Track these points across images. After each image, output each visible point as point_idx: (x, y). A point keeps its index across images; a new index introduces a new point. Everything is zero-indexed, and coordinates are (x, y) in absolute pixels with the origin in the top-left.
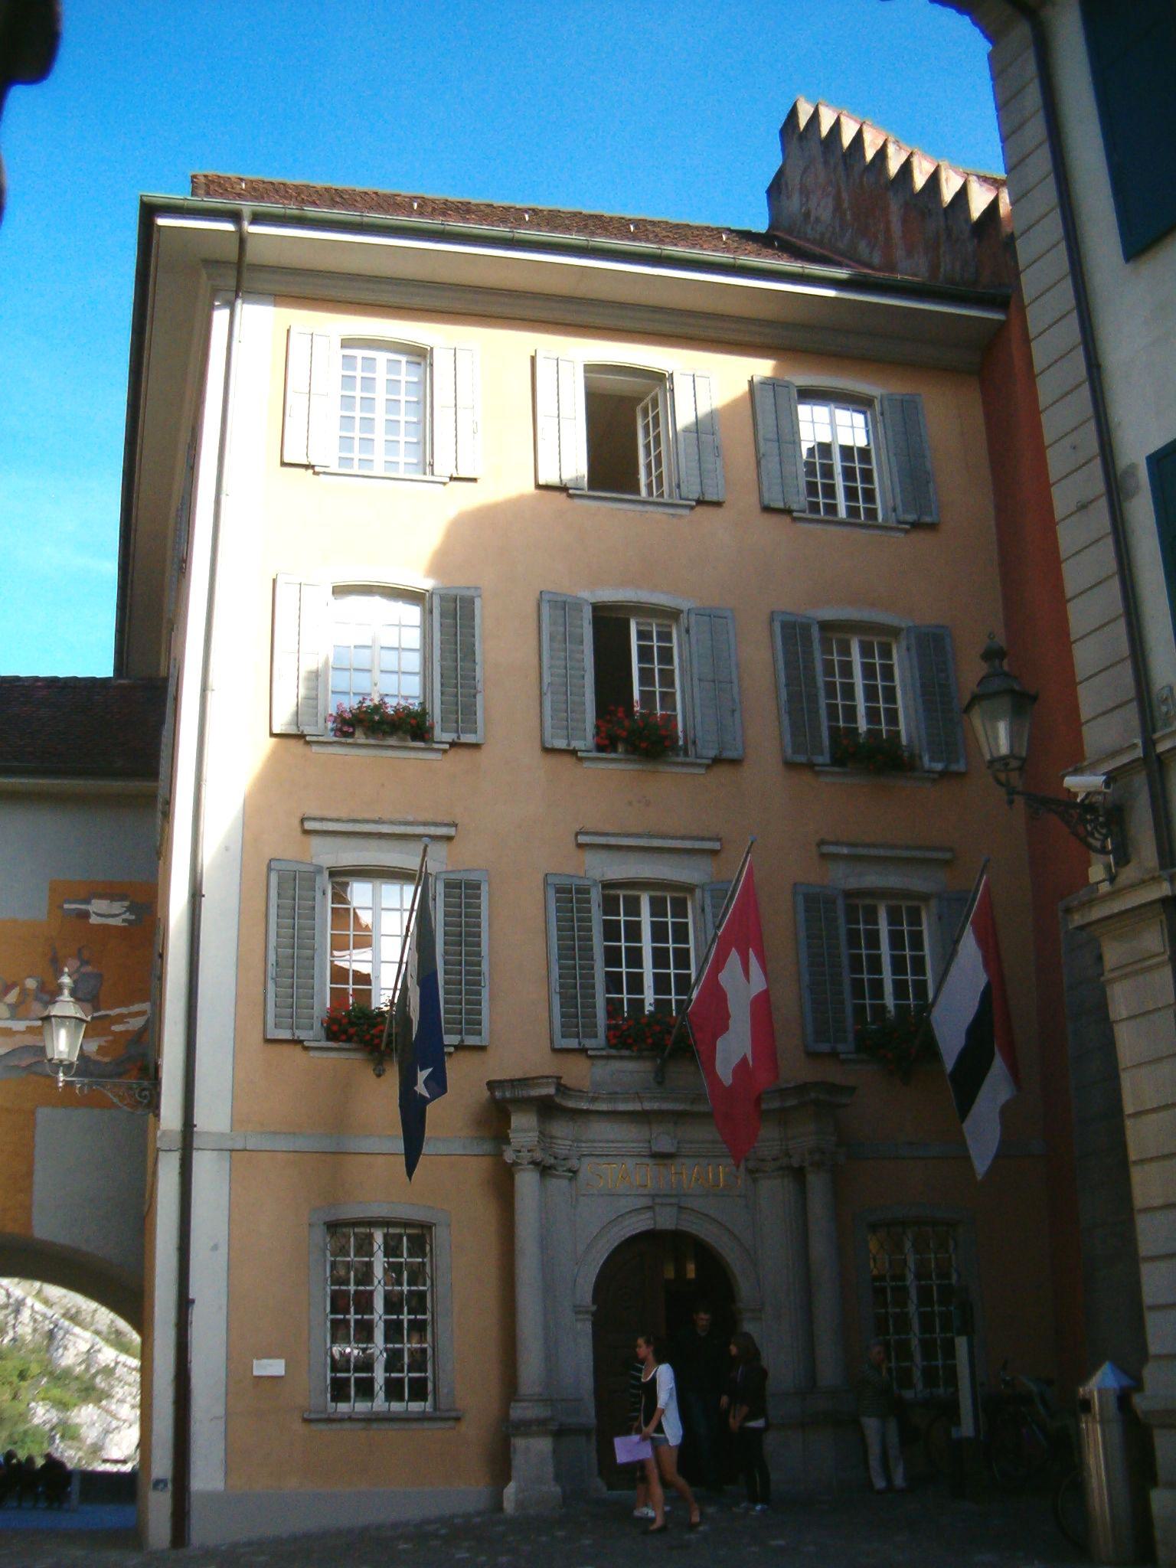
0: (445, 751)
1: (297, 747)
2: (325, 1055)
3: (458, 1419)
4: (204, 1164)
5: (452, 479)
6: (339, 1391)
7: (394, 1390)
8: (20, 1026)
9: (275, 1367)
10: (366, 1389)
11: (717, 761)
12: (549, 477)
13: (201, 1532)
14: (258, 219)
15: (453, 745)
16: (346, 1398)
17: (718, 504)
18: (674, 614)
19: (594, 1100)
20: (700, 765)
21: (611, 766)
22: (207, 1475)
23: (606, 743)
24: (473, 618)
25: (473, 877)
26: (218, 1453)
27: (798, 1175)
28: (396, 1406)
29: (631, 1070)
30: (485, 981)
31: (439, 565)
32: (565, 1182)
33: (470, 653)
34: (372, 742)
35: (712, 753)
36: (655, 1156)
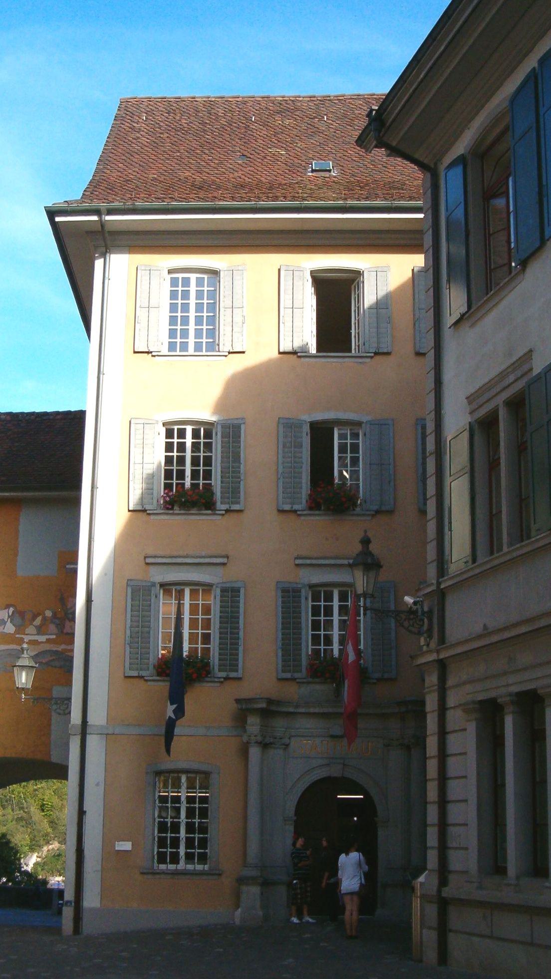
0: (223, 515)
1: (142, 516)
2: (156, 683)
3: (220, 875)
4: (93, 741)
5: (229, 353)
6: (162, 859)
7: (189, 857)
8: (42, 638)
9: (127, 846)
10: (175, 859)
11: (378, 512)
12: (286, 346)
13: (89, 926)
14: (110, 212)
15: (227, 511)
16: (165, 862)
17: (388, 354)
18: (359, 424)
19: (297, 707)
20: (368, 515)
21: (317, 518)
22: (91, 900)
23: (314, 505)
24: (240, 437)
25: (236, 585)
26: (98, 889)
27: (408, 748)
28: (190, 867)
29: (320, 689)
30: (241, 642)
31: (221, 405)
32: (281, 752)
33: (237, 458)
34: (182, 512)
35: (375, 508)
36: (332, 736)
